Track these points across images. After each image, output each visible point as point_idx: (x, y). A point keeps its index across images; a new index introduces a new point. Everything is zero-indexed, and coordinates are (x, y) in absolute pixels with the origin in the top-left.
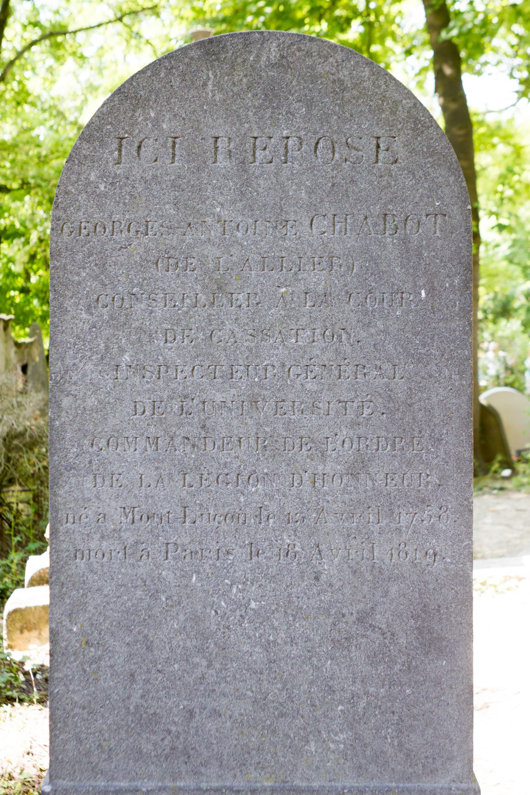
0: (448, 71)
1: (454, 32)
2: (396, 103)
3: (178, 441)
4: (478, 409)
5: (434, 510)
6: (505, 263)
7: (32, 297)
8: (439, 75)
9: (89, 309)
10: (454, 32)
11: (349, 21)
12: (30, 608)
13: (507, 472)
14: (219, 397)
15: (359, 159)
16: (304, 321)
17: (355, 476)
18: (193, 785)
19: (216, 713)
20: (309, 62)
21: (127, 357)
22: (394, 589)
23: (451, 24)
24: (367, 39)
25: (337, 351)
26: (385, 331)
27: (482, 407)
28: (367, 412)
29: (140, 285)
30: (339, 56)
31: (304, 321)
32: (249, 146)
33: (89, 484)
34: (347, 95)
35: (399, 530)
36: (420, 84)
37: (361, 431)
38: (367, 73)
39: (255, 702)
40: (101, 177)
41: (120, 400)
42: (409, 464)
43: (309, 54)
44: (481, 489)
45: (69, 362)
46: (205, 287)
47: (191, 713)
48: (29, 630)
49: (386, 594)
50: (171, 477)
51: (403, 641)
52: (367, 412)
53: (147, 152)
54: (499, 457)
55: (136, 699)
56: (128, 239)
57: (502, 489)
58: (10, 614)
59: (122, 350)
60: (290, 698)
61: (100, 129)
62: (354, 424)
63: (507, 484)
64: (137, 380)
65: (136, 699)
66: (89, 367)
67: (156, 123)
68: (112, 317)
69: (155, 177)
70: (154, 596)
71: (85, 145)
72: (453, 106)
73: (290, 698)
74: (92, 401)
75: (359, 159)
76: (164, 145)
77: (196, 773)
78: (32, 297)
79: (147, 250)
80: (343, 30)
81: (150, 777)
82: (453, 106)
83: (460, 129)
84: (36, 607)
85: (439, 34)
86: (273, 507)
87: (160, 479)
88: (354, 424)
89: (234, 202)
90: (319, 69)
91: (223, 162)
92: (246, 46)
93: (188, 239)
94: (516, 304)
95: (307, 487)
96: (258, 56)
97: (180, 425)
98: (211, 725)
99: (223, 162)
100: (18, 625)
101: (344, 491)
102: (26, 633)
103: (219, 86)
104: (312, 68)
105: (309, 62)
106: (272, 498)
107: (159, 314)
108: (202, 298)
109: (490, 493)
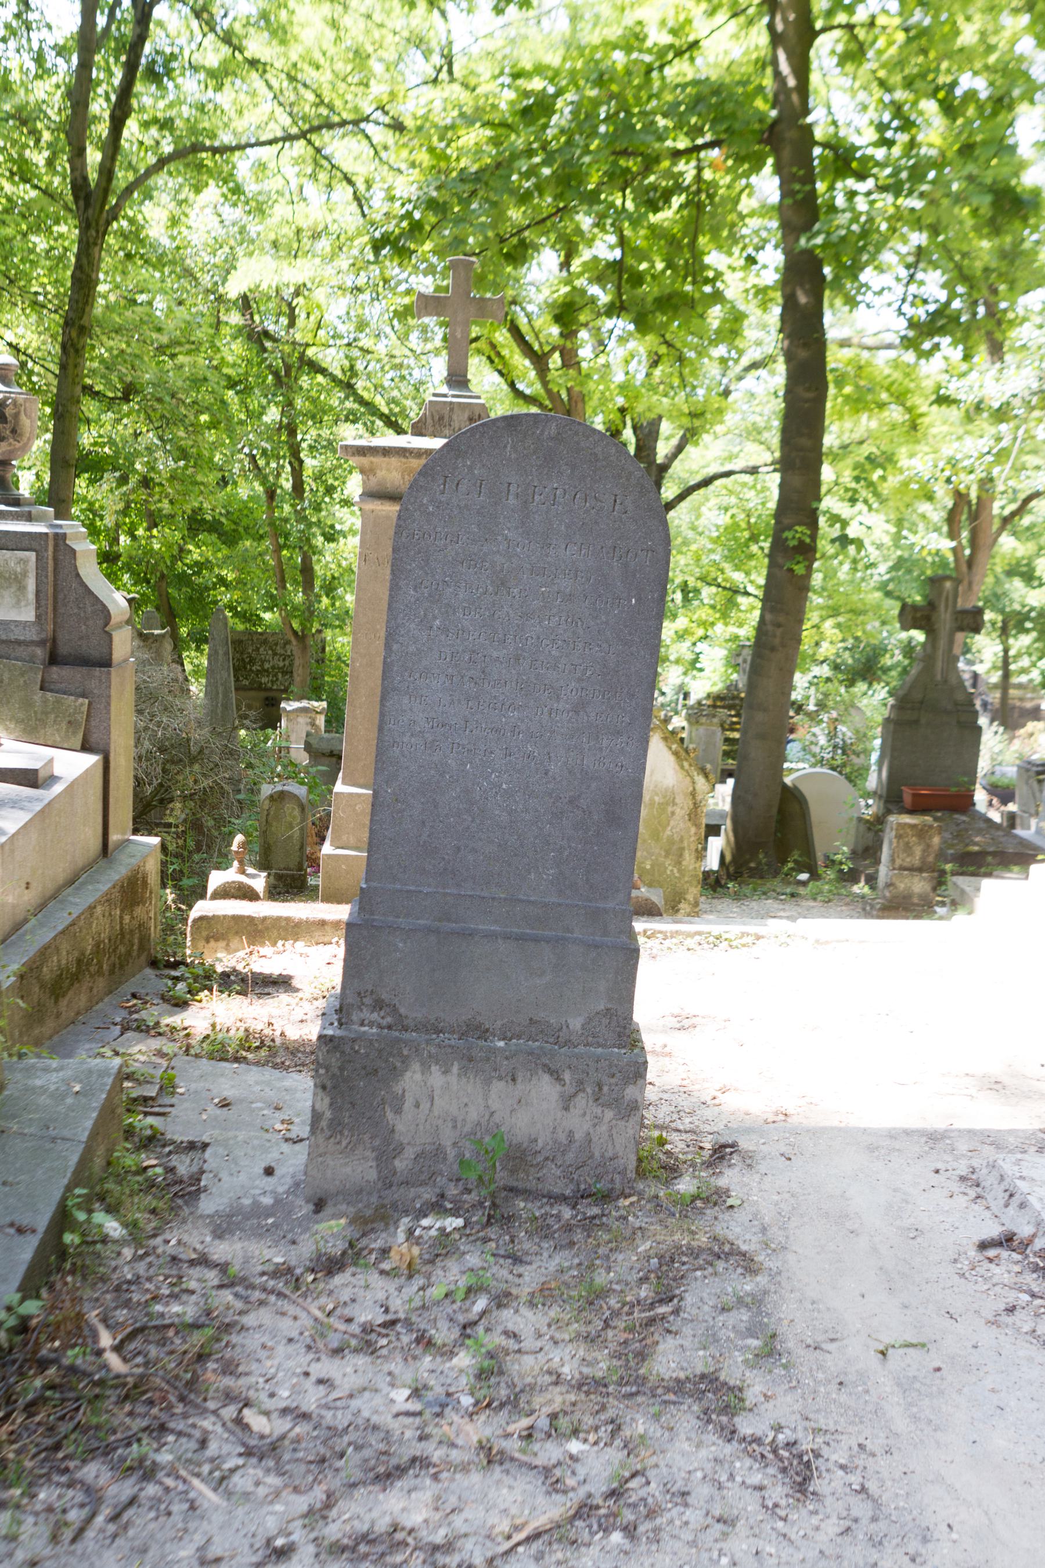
0: (803, 299)
1: (819, 240)
2: (631, 473)
3: (466, 679)
4: (779, 790)
5: (624, 739)
6: (878, 595)
7: (120, 569)
8: (790, 305)
9: (415, 589)
10: (819, 240)
11: (667, 196)
12: (218, 917)
13: (804, 876)
14: (495, 654)
15: (602, 508)
16: (555, 611)
17: (577, 713)
18: (455, 892)
19: (474, 850)
20: (576, 439)
21: (438, 622)
22: (594, 785)
23: (817, 226)
24: (693, 226)
25: (574, 633)
26: (607, 623)
27: (785, 786)
28: (589, 673)
29: (451, 576)
30: (596, 438)
31: (555, 611)
32: (530, 491)
33: (406, 701)
34: (599, 464)
35: (601, 749)
36: (667, 439)
37: (584, 685)
38: (613, 451)
39: (500, 845)
40: (431, 501)
41: (431, 649)
42: (612, 708)
43: (576, 433)
44: (764, 893)
45: (399, 621)
46: (493, 582)
47: (459, 849)
48: (217, 940)
49: (589, 787)
50: (459, 701)
51: (596, 817)
52: (589, 673)
53: (463, 488)
54: (796, 855)
55: (424, 837)
56: (445, 545)
57: (793, 895)
58: (195, 921)
59: (435, 618)
60: (522, 846)
61: (432, 469)
62: (580, 680)
63: (802, 891)
64: (443, 637)
65: (424, 837)
66: (413, 626)
67: (471, 468)
68: (430, 595)
69: (466, 506)
70: (442, 775)
71: (422, 479)
72: (803, 354)
73: (522, 846)
74: (412, 648)
75: (602, 508)
76: (475, 485)
77: (458, 885)
78: (120, 569)
79: (457, 554)
80: (656, 210)
81: (429, 885)
82: (803, 354)
83: (808, 389)
84: (225, 916)
85: (797, 240)
86: (523, 727)
87: (452, 702)
88: (580, 680)
89: (517, 528)
90: (582, 444)
91: (512, 501)
92: (535, 423)
93: (485, 549)
94: (887, 661)
95: (546, 716)
96: (543, 431)
97: (468, 669)
98: (470, 858)
99: (512, 501)
100: (205, 934)
101: (569, 721)
102: (212, 943)
103: (513, 447)
104: (578, 443)
105: (576, 439)
106: (523, 721)
107: (461, 596)
108: (490, 589)
109: (776, 899)
